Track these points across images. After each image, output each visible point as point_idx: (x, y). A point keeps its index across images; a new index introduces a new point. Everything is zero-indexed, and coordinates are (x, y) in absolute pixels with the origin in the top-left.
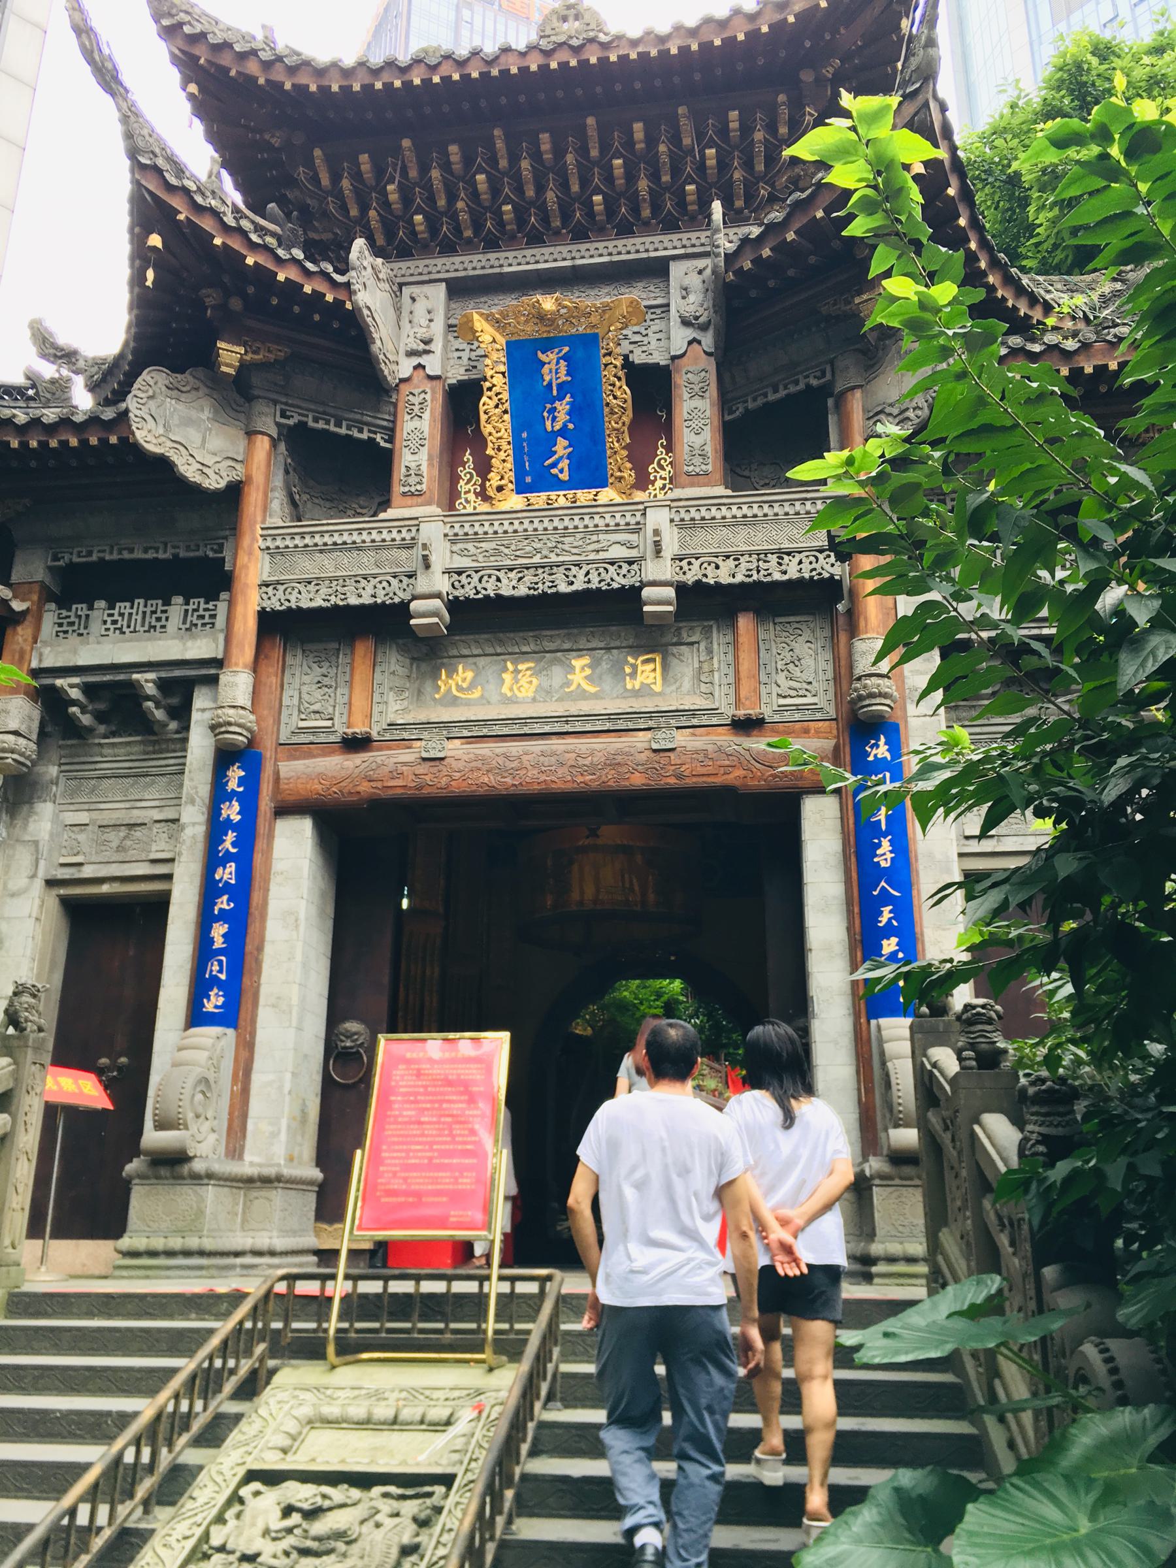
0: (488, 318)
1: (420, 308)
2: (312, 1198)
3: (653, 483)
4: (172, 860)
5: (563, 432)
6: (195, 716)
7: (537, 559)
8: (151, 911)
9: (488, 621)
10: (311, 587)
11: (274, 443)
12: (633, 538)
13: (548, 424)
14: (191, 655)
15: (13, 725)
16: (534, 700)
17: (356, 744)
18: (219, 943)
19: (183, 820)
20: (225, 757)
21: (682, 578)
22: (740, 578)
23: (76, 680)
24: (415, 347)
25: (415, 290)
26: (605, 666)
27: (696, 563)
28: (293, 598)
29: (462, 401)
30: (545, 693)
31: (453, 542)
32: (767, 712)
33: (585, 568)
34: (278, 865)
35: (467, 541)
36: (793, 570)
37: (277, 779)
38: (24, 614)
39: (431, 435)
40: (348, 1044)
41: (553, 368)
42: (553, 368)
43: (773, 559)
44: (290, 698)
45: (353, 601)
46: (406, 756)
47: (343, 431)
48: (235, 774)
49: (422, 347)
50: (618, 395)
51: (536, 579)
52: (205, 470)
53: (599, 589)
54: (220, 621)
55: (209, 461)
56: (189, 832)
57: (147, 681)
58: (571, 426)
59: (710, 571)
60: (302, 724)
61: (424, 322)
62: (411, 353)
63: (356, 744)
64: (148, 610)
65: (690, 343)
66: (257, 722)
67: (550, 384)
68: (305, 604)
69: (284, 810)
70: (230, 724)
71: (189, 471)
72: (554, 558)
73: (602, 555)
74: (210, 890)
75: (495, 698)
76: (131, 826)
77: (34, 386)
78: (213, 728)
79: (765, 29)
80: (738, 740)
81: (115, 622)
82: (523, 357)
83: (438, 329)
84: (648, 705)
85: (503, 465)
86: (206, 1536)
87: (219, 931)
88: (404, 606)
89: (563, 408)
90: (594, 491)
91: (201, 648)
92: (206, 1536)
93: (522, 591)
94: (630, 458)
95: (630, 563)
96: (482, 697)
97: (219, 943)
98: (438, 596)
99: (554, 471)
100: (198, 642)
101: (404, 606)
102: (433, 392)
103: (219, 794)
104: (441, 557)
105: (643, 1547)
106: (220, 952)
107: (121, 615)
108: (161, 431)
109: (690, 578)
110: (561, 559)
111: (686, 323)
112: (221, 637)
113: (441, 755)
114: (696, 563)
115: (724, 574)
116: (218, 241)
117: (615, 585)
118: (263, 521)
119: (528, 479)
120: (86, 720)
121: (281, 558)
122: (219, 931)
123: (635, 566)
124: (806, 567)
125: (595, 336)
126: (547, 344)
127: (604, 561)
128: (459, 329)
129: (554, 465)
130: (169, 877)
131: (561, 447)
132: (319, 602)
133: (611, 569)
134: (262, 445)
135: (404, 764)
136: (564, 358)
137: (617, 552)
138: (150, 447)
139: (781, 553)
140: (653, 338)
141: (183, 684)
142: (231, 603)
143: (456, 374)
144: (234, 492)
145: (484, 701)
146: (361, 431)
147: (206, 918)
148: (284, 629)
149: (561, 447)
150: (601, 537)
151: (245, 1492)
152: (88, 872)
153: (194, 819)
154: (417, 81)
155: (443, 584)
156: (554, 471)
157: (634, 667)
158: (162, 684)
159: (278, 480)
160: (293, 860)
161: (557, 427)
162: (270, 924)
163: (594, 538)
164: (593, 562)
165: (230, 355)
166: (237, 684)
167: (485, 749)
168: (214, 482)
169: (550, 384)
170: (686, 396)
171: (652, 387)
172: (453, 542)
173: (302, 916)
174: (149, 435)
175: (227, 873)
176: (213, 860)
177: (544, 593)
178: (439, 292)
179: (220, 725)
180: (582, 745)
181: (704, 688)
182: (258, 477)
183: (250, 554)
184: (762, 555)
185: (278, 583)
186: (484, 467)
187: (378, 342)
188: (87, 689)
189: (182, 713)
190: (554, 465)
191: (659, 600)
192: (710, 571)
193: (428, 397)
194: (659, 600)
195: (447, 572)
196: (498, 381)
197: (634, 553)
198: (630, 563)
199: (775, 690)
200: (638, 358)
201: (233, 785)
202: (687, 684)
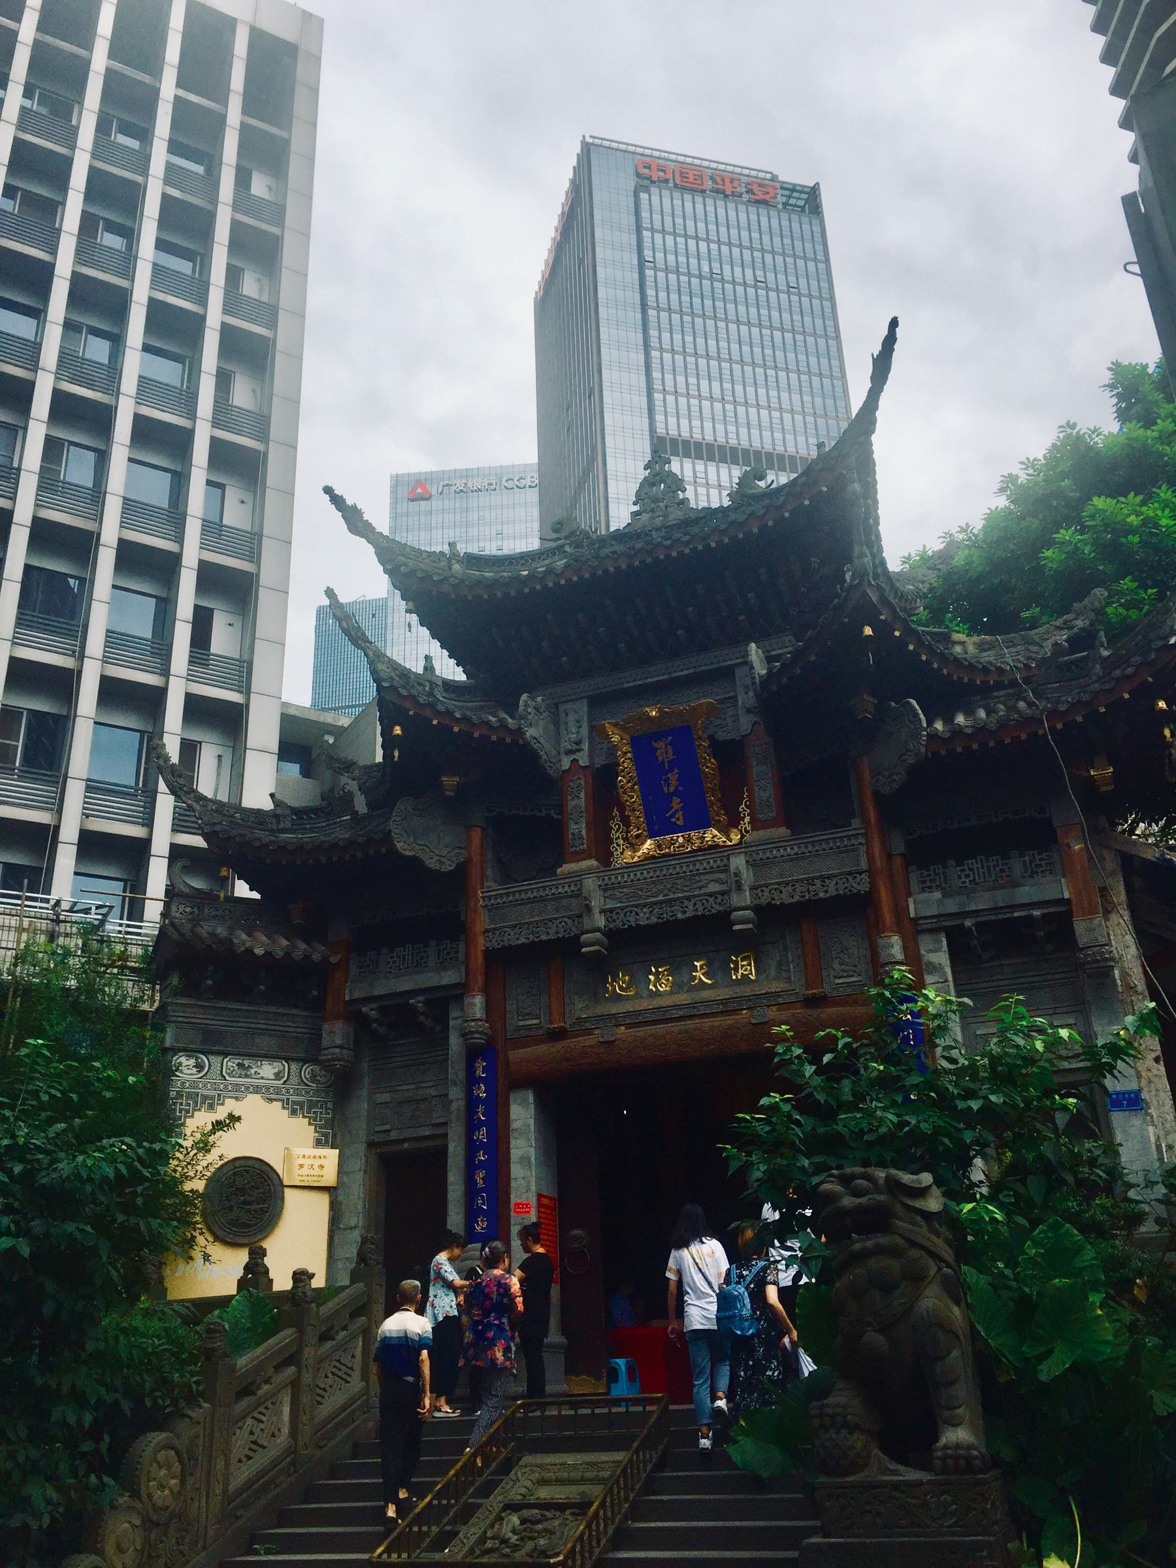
0: (616, 725)
1: (571, 719)
2: (562, 1357)
3: (743, 819)
4: (445, 1124)
5: (676, 793)
6: (451, 1023)
7: (660, 898)
8: (433, 1160)
9: (636, 945)
10: (517, 930)
11: (483, 829)
12: (723, 876)
13: (665, 789)
14: (444, 982)
15: (339, 1042)
16: (671, 993)
17: (557, 1035)
18: (480, 1182)
19: (451, 1097)
20: (472, 1054)
21: (757, 902)
22: (796, 898)
23: (373, 1006)
24: (569, 747)
25: (568, 706)
26: (717, 964)
27: (766, 890)
28: (505, 939)
29: (603, 780)
30: (677, 987)
31: (605, 890)
32: (827, 989)
33: (693, 901)
34: (515, 1125)
35: (613, 888)
36: (833, 888)
37: (507, 1063)
38: (338, 964)
39: (586, 807)
40: (576, 1246)
41: (663, 751)
42: (663, 751)
43: (818, 882)
44: (511, 1006)
45: (544, 938)
46: (590, 1041)
47: (528, 813)
48: (480, 1065)
49: (575, 747)
50: (709, 766)
51: (661, 911)
52: (443, 859)
53: (703, 915)
54: (461, 956)
55: (445, 852)
56: (454, 1106)
57: (418, 1002)
58: (681, 788)
59: (776, 895)
60: (521, 1023)
61: (574, 730)
62: (569, 752)
63: (557, 1035)
64: (991, 863)
65: (753, 725)
66: (490, 1027)
67: (663, 762)
68: (515, 943)
69: (518, 1083)
70: (473, 1033)
71: (432, 863)
72: (672, 896)
73: (704, 891)
74: (472, 1147)
75: (646, 993)
76: (418, 1101)
77: (329, 805)
78: (463, 1035)
79: (770, 523)
80: (809, 1012)
81: (967, 876)
82: (642, 746)
83: (585, 731)
84: (746, 991)
85: (638, 817)
86: (485, 1532)
87: (480, 1176)
88: (727, 914)
89: (673, 777)
90: (702, 831)
91: (449, 977)
92: (485, 1532)
93: (654, 920)
94: (723, 807)
95: (723, 895)
96: (637, 993)
97: (480, 1182)
98: (598, 930)
99: (673, 820)
100: (449, 973)
101: (727, 914)
102: (586, 777)
103: (471, 1080)
104: (597, 902)
105: (301, 1277)
106: (482, 1190)
107: (399, 957)
108: (412, 839)
109: (764, 901)
110: (677, 895)
111: (748, 711)
112: (463, 968)
113: (612, 1039)
114: (766, 890)
115: (785, 897)
116: (435, 722)
117: (714, 911)
118: (482, 887)
119: (657, 827)
120: (382, 1030)
121: (501, 913)
122: (480, 1176)
123: (726, 897)
124: (841, 887)
125: (689, 727)
126: (658, 736)
127: (705, 894)
128: (597, 732)
129: (673, 816)
130: (446, 1135)
131: (676, 803)
132: (523, 940)
133: (711, 900)
134: (476, 834)
135: (590, 1046)
136: (670, 743)
137: (713, 887)
138: (407, 853)
139: (823, 878)
140: (729, 720)
141: (444, 1001)
142: (467, 946)
143: (600, 761)
144: (462, 869)
145: (638, 996)
146: (540, 811)
147: (471, 1167)
148: (505, 964)
149: (676, 803)
150: (702, 877)
151: (503, 1514)
152: (394, 1135)
153: (456, 1094)
154: (551, 584)
155: (601, 921)
156: (673, 820)
157: (736, 963)
158: (427, 1003)
159: (489, 855)
160: (522, 1114)
161: (672, 789)
162: (513, 1167)
163: (697, 878)
164: (699, 895)
165: (449, 781)
166: (477, 1004)
167: (641, 1032)
168: (448, 867)
169: (663, 762)
170: (754, 764)
171: (731, 755)
172: (605, 890)
173: (533, 1159)
174: (403, 846)
175: (482, 1134)
176: (471, 1126)
177: (668, 921)
178: (584, 707)
179: (467, 1034)
180: (707, 1023)
181: (784, 974)
182: (476, 858)
183: (476, 911)
184: (810, 881)
185: (495, 929)
186: (626, 821)
187: (544, 757)
188: (380, 1010)
189: (443, 1020)
190: (673, 816)
191: (743, 920)
192: (776, 895)
193: (582, 782)
194: (743, 920)
195: (603, 911)
196: (626, 763)
197: (724, 887)
198: (723, 895)
199: (832, 972)
200: (721, 736)
201: (480, 1073)
202: (773, 972)
